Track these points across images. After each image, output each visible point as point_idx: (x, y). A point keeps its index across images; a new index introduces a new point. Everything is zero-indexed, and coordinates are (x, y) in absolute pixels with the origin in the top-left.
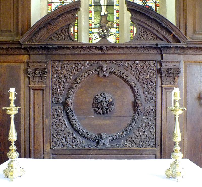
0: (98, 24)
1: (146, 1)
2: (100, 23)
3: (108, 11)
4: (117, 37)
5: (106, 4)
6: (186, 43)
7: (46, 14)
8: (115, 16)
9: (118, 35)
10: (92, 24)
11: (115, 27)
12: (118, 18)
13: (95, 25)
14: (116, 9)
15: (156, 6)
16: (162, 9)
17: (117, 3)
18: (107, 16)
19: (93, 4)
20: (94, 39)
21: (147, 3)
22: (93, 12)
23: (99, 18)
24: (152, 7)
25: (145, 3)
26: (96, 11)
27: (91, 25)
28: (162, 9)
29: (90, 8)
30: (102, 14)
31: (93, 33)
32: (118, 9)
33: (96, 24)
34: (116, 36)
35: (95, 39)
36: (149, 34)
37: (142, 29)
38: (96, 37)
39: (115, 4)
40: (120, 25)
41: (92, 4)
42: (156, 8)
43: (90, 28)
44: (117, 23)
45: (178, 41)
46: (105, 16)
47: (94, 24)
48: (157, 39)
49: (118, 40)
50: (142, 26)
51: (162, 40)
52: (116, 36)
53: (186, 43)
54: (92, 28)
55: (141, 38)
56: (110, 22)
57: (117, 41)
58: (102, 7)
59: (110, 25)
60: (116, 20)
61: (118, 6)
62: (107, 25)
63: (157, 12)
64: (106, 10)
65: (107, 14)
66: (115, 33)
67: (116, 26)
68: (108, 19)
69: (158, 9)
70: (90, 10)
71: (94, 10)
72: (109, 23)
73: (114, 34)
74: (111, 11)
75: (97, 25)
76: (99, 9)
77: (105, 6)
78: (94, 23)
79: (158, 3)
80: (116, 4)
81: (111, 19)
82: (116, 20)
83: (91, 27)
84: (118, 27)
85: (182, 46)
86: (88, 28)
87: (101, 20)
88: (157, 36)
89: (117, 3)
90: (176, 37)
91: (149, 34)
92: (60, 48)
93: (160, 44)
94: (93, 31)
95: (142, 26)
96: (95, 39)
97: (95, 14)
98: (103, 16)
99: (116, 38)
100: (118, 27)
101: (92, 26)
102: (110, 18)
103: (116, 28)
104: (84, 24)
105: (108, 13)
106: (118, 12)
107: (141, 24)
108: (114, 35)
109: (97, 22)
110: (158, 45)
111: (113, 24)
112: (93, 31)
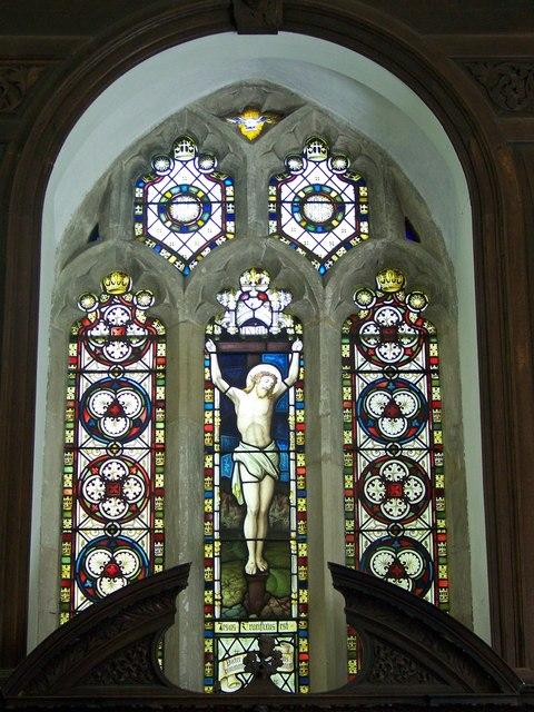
0: (235, 605)
1: (401, 445)
2: (241, 602)
3: (271, 559)
4: (301, 650)
5: (261, 536)
6: (517, 693)
7: (54, 629)
8: (295, 578)
9: (303, 643)
10: (213, 606)
11: (294, 615)
12: (303, 585)
13: (224, 610)
14: (297, 554)
15: (436, 542)
16: (456, 553)
17: (301, 532)
18: (267, 577)
19: (217, 535)
20: (220, 658)
21: (402, 449)
22: (217, 561)
23: (238, 584)
24: (423, 543)
25: (398, 450)
26: (227, 559)
27: (211, 608)
28: (456, 553)
29: (208, 548)
30: (250, 568)
31: (217, 637)
32: (303, 553)
33: (229, 603)
34: (297, 646)
35: (223, 659)
36: (403, 663)
37: (381, 646)
38: (227, 652)
39: (293, 535)
40: (311, 607)
41: (213, 535)
42: (436, 549)
43: (206, 621)
44: (301, 601)
45: (495, 688)
46: (260, 577)
47: (222, 606)
48: (428, 678)
49: (306, 661)
50: (379, 638)
51: (445, 682)
52: (297, 646)
53: (517, 693)
54: (213, 620)
55: (378, 675)
56: (276, 598)
57: (304, 690)
58: (250, 545)
59: (278, 610)
60: (298, 592)
61: (304, 541)
62: (267, 607)
63: (443, 607)
64: (264, 558)
65: (267, 571)
66: (293, 638)
67: (299, 612)
68: (269, 587)
69: (443, 598)
70: (209, 555)
71: (219, 511)
72: (274, 603)
73: (289, 639)
74: (279, 561)
75: (231, 608)
76: (240, 555)
77: (260, 544)
78: (221, 600)
79: (441, 529)
80: (297, 534)
81: (281, 589)
82: (298, 592)
83: (209, 616)
84: (303, 615)
85: (506, 701)
86: (201, 621)
87: (245, 593)
88: (427, 669)
89: (301, 532)
90: (488, 674)
91: (403, 663)
92: (65, 265)
93: (439, 697)
94: (217, 630)
95: (379, 638)
96: (223, 659)
97: (225, 571)
98: (252, 576)
99: (300, 653)
100: (303, 615)
101: (213, 613)
102: (275, 584)
103: (298, 620)
104: (187, 608)
105: (269, 567)
106: (303, 561)
107: (379, 632)
108: (290, 643)
109: (232, 597)
110: (432, 701)
111: (288, 604)
112: (217, 630)
